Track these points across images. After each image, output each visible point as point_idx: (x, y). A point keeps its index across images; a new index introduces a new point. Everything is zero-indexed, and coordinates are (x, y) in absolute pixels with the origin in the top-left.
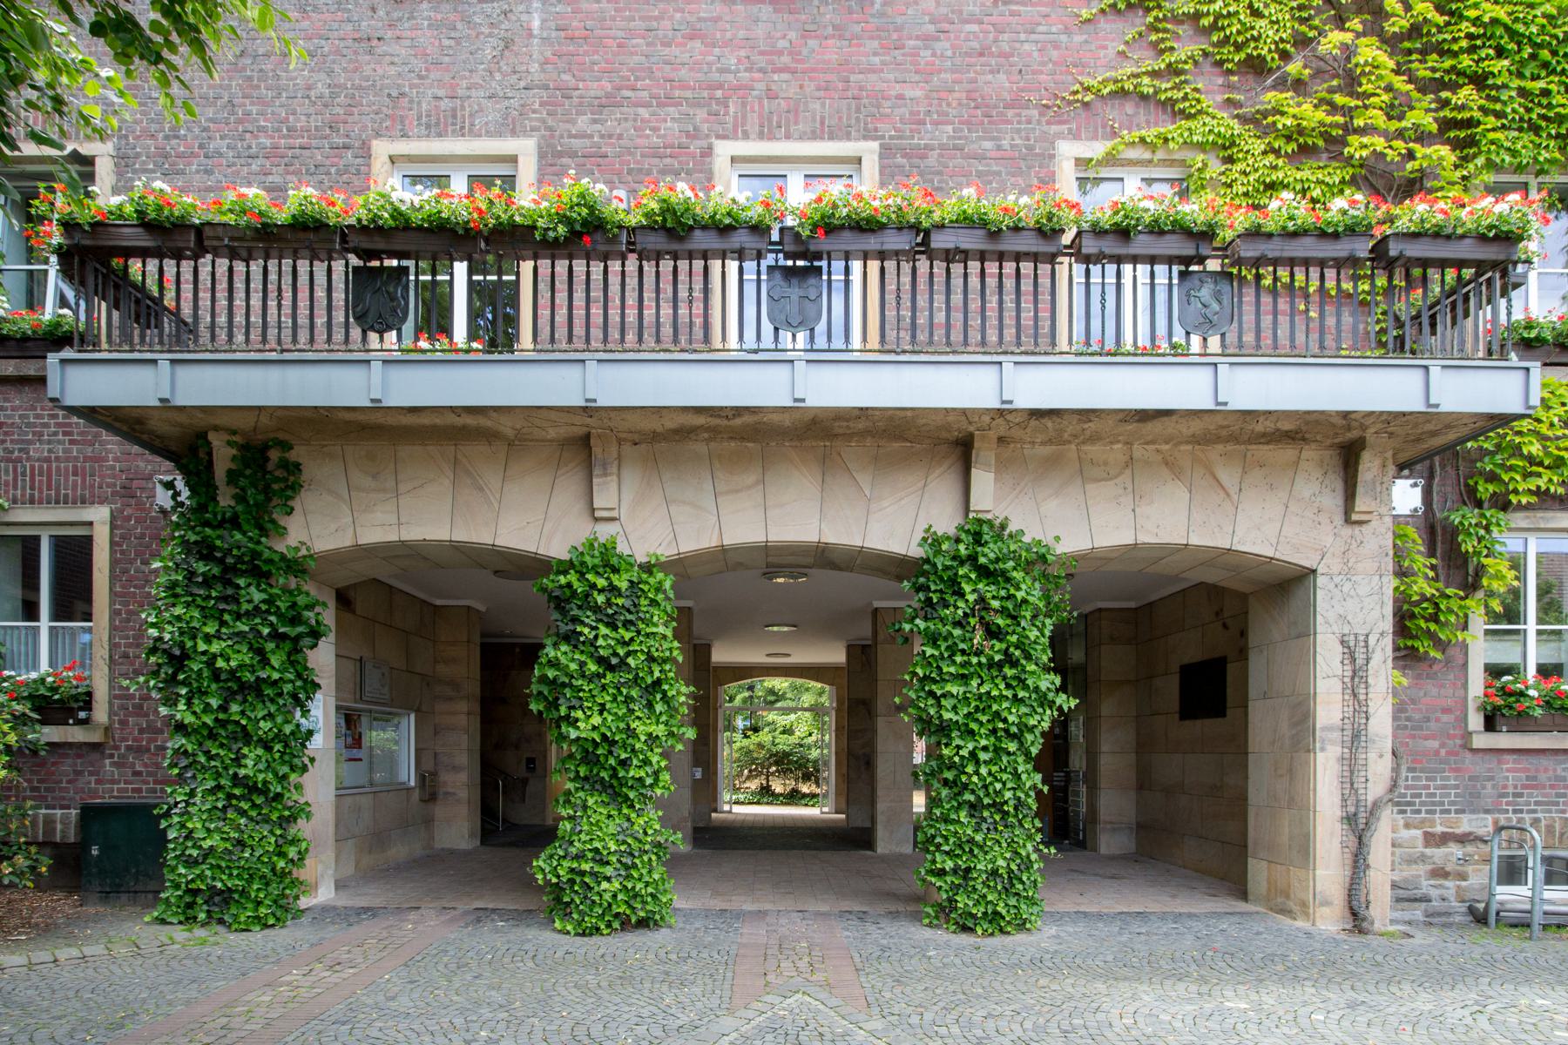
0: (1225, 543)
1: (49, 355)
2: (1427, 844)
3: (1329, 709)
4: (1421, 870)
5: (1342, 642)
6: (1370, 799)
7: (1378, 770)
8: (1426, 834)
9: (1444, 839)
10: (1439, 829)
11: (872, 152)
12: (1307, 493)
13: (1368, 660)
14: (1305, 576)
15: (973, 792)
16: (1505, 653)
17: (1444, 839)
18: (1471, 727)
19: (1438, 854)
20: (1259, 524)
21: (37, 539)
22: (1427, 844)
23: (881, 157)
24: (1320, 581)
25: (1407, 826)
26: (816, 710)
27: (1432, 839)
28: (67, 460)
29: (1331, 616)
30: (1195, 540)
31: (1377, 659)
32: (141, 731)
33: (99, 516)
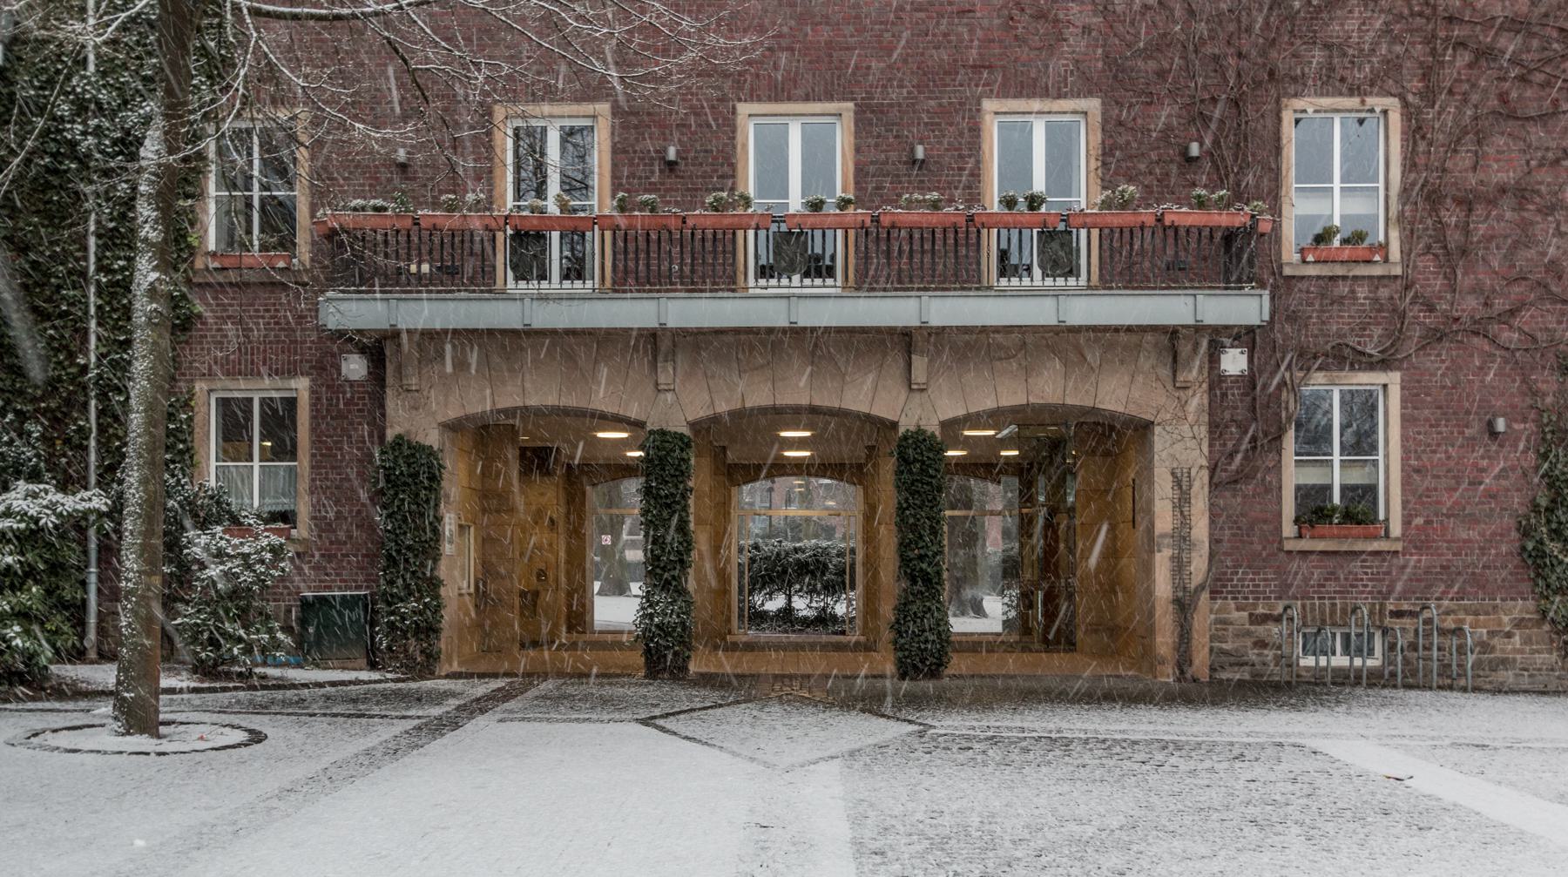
0: (1088, 403)
1: (998, 628)
2: (1251, 623)
3: (1164, 521)
4: (1249, 642)
5: (1173, 474)
6: (1193, 586)
7: (1199, 566)
8: (1251, 615)
9: (1265, 619)
10: (1260, 611)
11: (847, 110)
12: (1147, 366)
13: (1190, 487)
14: (1143, 429)
15: (972, 31)
16: (1312, 477)
17: (1265, 619)
18: (1285, 534)
19: (1260, 630)
20: (1115, 393)
21: (250, 400)
22: (1251, 623)
23: (856, 113)
24: (1157, 430)
25: (1238, 609)
26: (750, 493)
27: (1256, 620)
28: (278, 342)
29: (1164, 454)
30: (1069, 401)
31: (1197, 485)
32: (331, 543)
33: (301, 386)
